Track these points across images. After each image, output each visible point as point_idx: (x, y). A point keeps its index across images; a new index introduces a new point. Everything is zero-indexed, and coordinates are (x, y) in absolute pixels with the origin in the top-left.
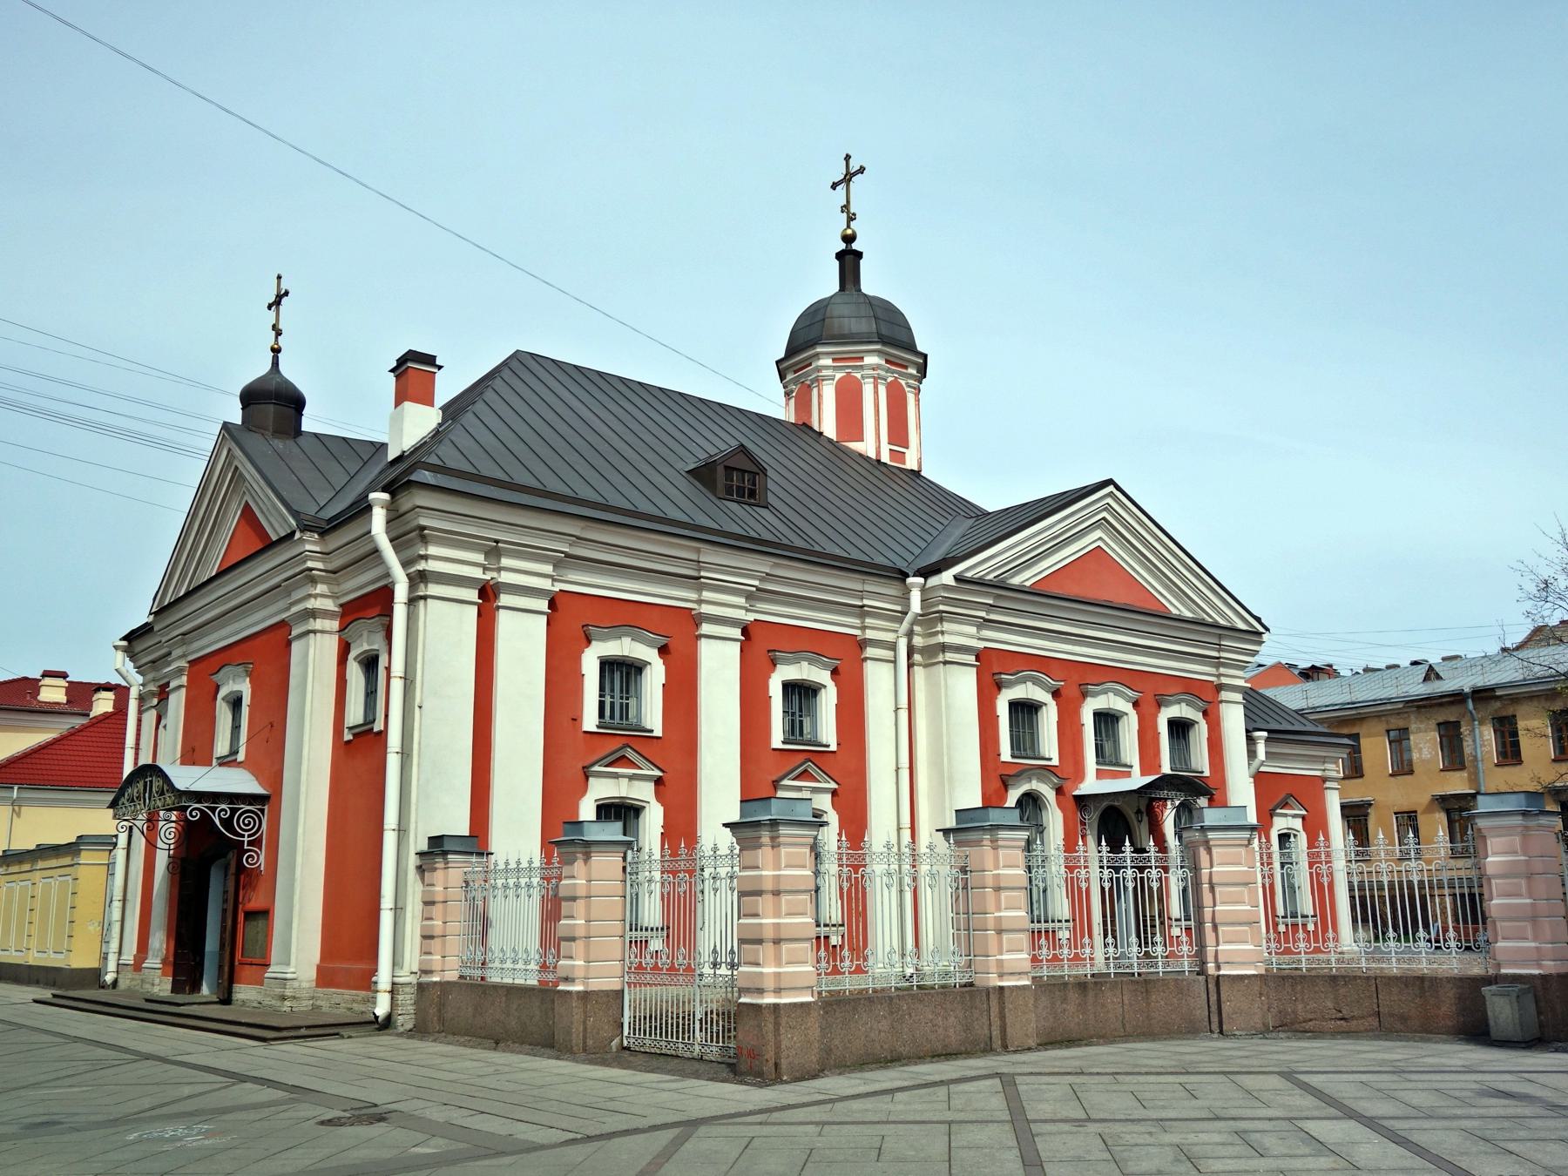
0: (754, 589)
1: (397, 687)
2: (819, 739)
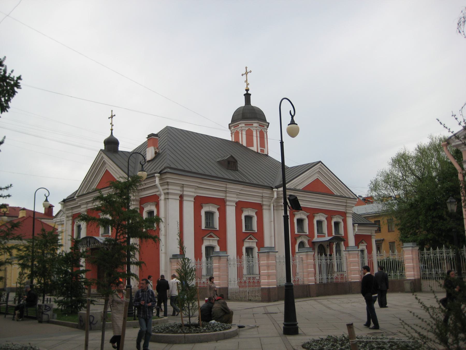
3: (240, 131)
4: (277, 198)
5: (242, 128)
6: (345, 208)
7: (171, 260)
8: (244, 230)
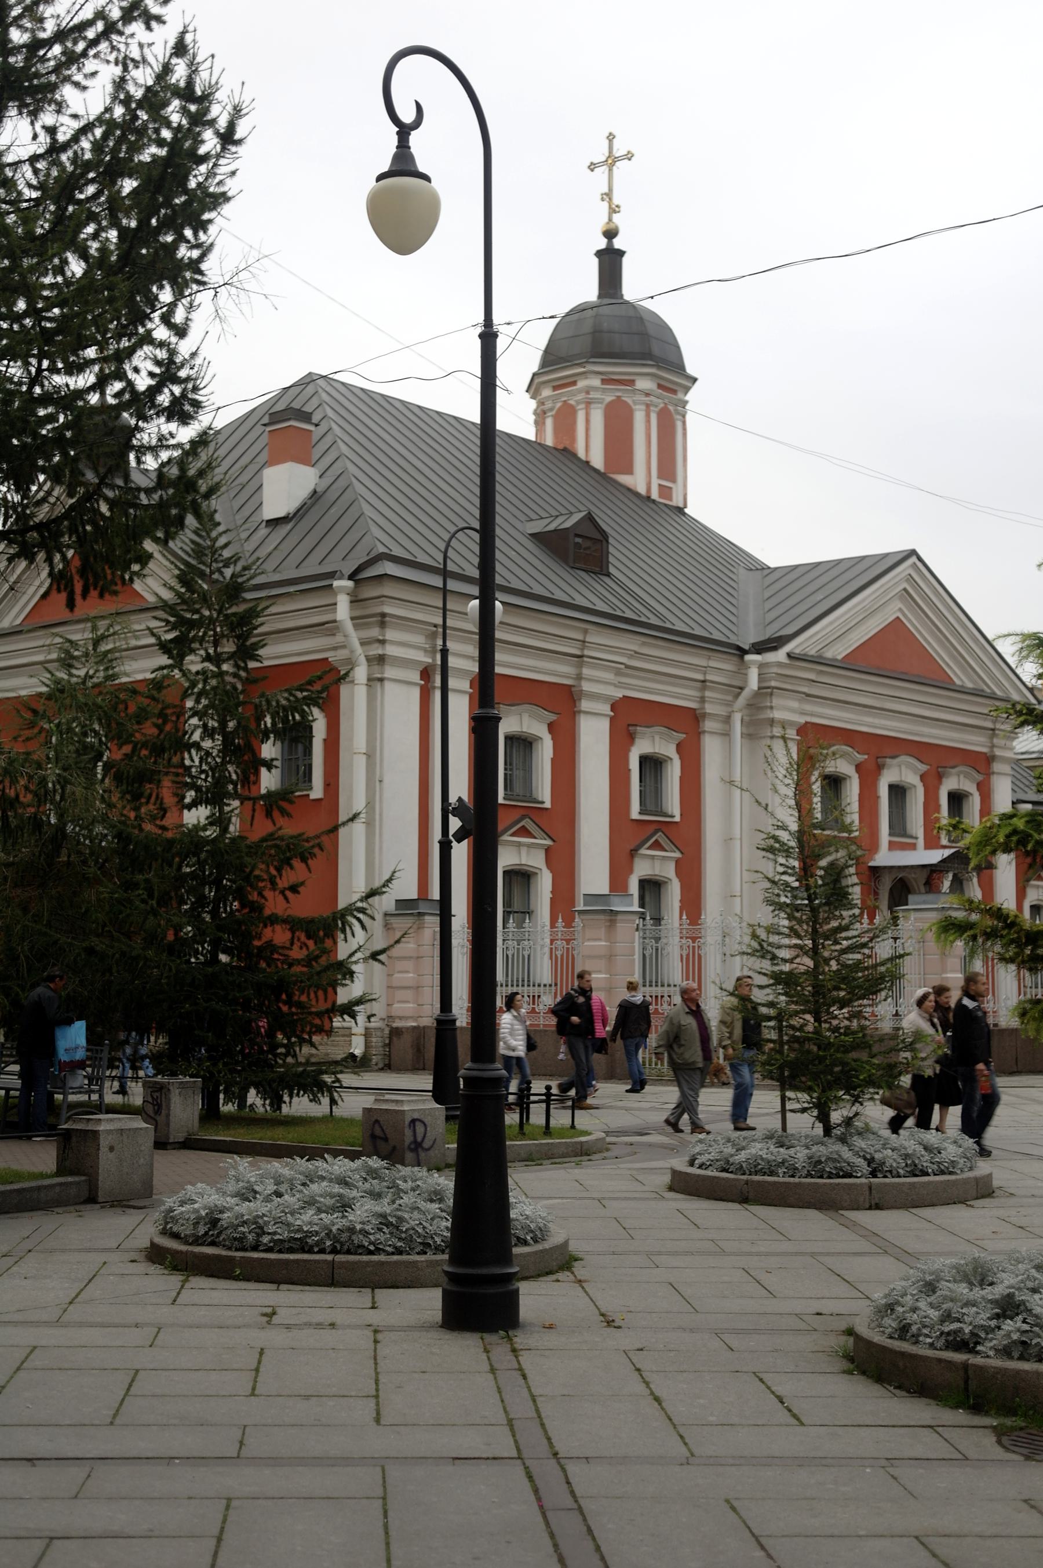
0: (622, 666)
1: (360, 764)
2: (664, 810)
3: (583, 406)
4: (759, 688)
5: (588, 393)
6: (698, 694)
7: (393, 920)
8: (635, 813)
